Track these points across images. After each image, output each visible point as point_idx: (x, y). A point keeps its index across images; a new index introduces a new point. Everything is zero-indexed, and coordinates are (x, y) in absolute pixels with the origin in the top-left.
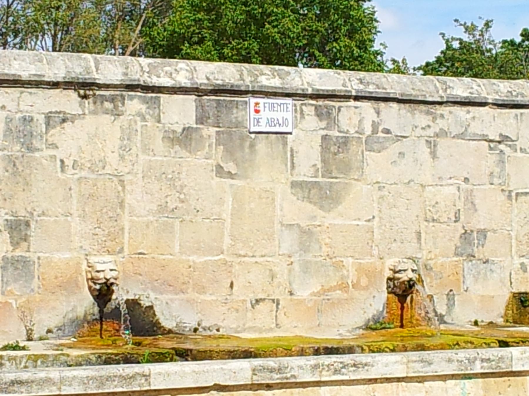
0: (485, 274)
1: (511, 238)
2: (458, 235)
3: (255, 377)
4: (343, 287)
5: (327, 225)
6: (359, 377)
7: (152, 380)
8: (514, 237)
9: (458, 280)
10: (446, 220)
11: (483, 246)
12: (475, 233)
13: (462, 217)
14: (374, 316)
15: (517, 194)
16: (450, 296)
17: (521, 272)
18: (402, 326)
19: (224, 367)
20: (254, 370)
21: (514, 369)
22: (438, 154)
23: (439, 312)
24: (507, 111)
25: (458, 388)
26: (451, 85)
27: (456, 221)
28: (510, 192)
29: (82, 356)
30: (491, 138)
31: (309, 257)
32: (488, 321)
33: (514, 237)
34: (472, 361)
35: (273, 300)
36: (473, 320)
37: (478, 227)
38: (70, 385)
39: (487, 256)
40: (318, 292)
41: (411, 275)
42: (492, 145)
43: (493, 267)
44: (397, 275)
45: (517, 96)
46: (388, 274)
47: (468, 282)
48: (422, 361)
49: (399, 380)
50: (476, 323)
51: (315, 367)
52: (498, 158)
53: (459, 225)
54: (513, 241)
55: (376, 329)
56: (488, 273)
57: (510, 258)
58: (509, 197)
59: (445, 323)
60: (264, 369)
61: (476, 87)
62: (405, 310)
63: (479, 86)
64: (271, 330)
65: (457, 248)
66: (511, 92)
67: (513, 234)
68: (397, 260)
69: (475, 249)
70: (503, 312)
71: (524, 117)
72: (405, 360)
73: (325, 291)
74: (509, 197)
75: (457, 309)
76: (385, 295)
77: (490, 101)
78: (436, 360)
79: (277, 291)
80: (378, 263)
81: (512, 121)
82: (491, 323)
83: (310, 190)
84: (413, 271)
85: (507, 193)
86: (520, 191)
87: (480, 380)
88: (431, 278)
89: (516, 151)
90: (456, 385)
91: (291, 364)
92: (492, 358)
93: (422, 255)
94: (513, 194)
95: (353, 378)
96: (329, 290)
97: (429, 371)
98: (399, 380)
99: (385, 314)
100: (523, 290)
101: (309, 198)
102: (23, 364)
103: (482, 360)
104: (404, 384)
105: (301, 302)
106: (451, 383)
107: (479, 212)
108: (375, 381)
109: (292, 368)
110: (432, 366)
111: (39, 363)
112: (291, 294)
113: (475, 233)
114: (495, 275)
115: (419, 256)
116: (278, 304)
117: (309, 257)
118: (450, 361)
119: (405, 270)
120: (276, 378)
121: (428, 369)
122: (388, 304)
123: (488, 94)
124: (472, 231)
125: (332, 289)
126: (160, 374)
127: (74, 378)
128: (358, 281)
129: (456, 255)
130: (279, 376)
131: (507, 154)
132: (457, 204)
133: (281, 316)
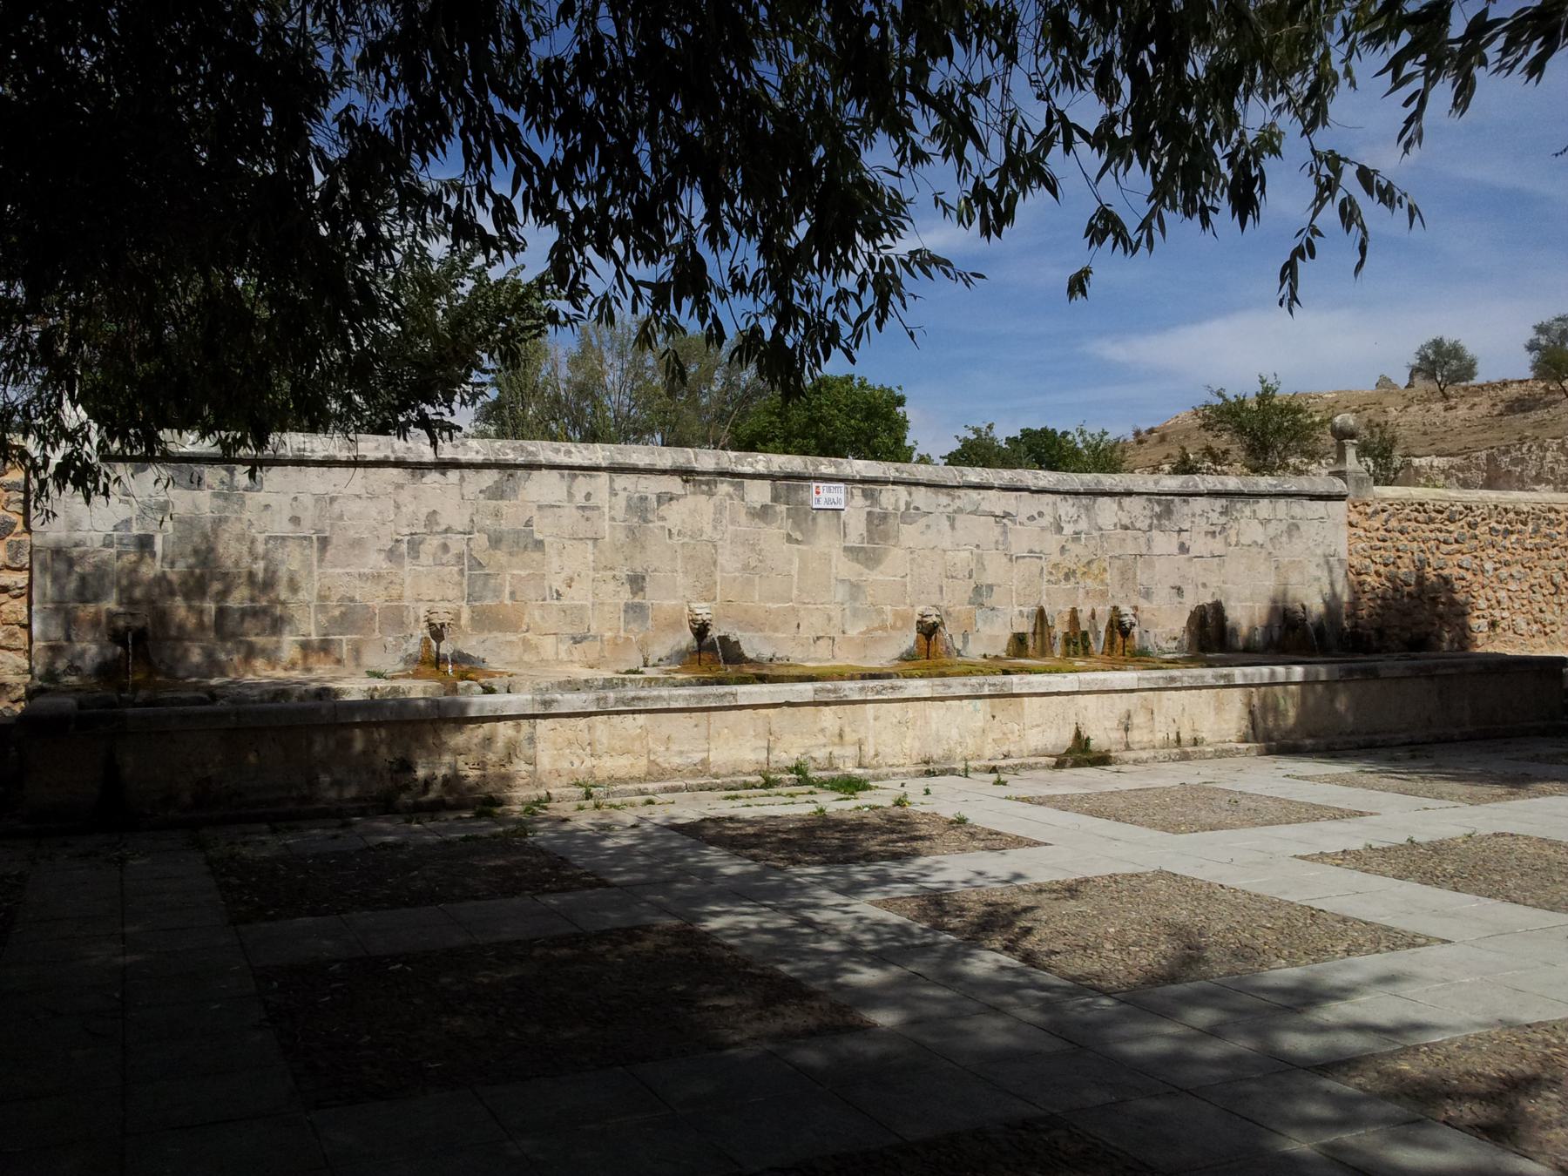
4: (883, 628)
16: (965, 636)
31: (857, 605)
34: (981, 686)
41: (935, 619)
46: (918, 618)
49: (926, 699)
51: (862, 689)
60: (823, 690)
73: (869, 631)
75: (970, 645)
76: (915, 634)
97: (949, 692)
98: (926, 699)
105: (851, 639)
106: (965, 702)
117: (857, 605)
120: (832, 697)
122: (917, 641)
125: (876, 629)
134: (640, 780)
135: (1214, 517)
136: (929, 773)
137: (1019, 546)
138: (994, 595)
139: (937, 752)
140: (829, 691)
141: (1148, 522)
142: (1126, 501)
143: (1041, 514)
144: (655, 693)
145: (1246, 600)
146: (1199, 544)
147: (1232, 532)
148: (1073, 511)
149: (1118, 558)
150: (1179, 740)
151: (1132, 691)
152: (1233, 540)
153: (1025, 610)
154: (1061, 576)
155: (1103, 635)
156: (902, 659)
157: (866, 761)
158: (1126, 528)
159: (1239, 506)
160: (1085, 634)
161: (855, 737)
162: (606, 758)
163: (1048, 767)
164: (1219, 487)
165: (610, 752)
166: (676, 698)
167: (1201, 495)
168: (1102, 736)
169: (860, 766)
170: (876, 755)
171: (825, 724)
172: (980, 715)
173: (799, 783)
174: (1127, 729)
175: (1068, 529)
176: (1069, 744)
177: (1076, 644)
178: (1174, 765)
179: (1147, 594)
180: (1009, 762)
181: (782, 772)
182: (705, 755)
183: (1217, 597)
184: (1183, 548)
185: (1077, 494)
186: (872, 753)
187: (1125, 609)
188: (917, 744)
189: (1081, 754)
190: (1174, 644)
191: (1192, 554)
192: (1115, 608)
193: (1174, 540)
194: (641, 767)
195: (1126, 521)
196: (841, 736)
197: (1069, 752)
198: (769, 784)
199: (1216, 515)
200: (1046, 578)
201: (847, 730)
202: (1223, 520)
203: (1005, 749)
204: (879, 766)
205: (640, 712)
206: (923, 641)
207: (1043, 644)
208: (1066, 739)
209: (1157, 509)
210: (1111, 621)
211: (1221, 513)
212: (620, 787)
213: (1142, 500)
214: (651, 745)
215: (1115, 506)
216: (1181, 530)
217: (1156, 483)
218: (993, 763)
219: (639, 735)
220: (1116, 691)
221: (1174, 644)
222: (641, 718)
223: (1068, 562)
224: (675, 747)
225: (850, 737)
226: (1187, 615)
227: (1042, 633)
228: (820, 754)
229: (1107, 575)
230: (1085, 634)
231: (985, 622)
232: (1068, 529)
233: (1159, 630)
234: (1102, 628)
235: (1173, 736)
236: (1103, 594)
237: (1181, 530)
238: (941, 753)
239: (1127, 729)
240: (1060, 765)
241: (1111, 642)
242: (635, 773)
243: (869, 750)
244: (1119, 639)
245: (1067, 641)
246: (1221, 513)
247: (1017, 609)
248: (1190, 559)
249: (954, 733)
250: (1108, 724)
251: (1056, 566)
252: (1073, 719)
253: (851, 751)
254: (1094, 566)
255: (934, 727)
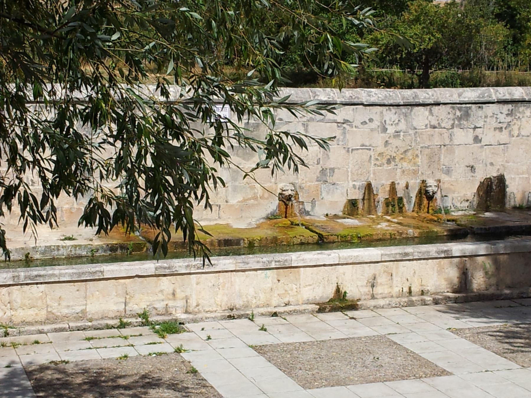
0: (333, 190)
1: (348, 172)
2: (318, 171)
3: (157, 271)
4: (255, 198)
5: (246, 167)
6: (210, 271)
7: (105, 274)
8: (350, 171)
9: (318, 194)
10: (312, 163)
11: (332, 176)
12: (328, 170)
13: (321, 162)
14: (271, 212)
15: (352, 150)
16: (313, 202)
17: (353, 189)
18: (286, 217)
19: (141, 267)
20: (156, 268)
21: (293, 265)
22: (309, 130)
23: (307, 210)
24: (348, 107)
25: (263, 275)
26: (318, 94)
27: (317, 164)
28: (348, 148)
29: (99, 245)
30: (338, 121)
31: (237, 184)
32: (334, 214)
33: (350, 171)
34: (270, 262)
35: (217, 205)
36: (326, 213)
37: (330, 167)
38: (64, 277)
39: (334, 181)
40: (241, 201)
41: (290, 192)
42: (339, 125)
43: (337, 187)
44: (284, 192)
45: (355, 99)
46: (279, 191)
47: (323, 195)
48: (243, 262)
49: (232, 271)
50: (327, 215)
51: (188, 266)
52: (343, 131)
53: (319, 166)
54: (349, 173)
55: (271, 219)
56: (335, 190)
57: (347, 182)
58: (348, 151)
59: (310, 215)
60: (161, 267)
61: (332, 94)
62: (288, 209)
63: (334, 94)
64: (216, 220)
65: (318, 178)
66: (351, 97)
67: (349, 170)
68: (284, 184)
69: (328, 178)
70: (342, 209)
71: (358, 110)
72: (234, 262)
73: (245, 200)
74: (348, 151)
75: (317, 208)
76: (277, 202)
77: (338, 102)
78: (251, 262)
79: (219, 201)
80: (274, 186)
81: (351, 112)
82: (336, 215)
83: (238, 151)
84: (291, 190)
85: (347, 149)
86: (354, 148)
87: (275, 270)
88: (303, 193)
89: (352, 127)
90: (262, 273)
91: (175, 265)
92: (281, 260)
93: (299, 182)
94: (350, 150)
95: (207, 271)
96: (247, 200)
97: (247, 267)
98: (232, 271)
99: (277, 211)
100: (354, 198)
101: (237, 154)
102: (69, 250)
103: (276, 262)
104: (234, 273)
105: (232, 206)
106: (259, 272)
107: (331, 159)
108: (219, 272)
109: (176, 267)
110: (249, 265)
111: (77, 249)
112: (227, 202)
113: (328, 170)
114: (339, 191)
115: (297, 182)
116: (220, 207)
117: (237, 184)
118: (258, 262)
119: (287, 190)
120: (167, 272)
121: (247, 266)
122: (279, 206)
123: (338, 98)
124: (326, 169)
125: (249, 199)
126: (109, 271)
127: (66, 273)
128: (263, 195)
129: (317, 181)
130: (169, 271)
131: (347, 129)
132: (319, 155)
133: (221, 213)
134: (41, 323)
135: (502, 118)
136: (230, 317)
137: (354, 141)
138: (335, 175)
139: (239, 303)
140: (165, 268)
141: (451, 122)
142: (435, 109)
143: (371, 120)
144: (51, 272)
145: (523, 174)
146: (489, 136)
147: (515, 128)
148: (395, 118)
149: (428, 147)
150: (410, 292)
151: (378, 262)
152: (516, 133)
153: (358, 184)
154: (384, 161)
155: (414, 199)
156: (268, 218)
157: (191, 309)
158: (435, 127)
159: (521, 109)
160: (401, 199)
161: (183, 295)
162: (20, 310)
163: (312, 312)
164: (508, 97)
165: (22, 307)
166: (64, 275)
167: (493, 103)
168: (353, 290)
169: (186, 312)
170: (198, 305)
171: (163, 288)
172: (269, 280)
173: (143, 324)
174: (373, 286)
175: (391, 130)
176: (332, 296)
177: (393, 206)
178: (399, 311)
179: (448, 171)
180: (288, 308)
181: (133, 316)
182: (84, 307)
183: (501, 172)
184: (477, 140)
185: (398, 105)
186: (195, 304)
187: (431, 182)
188: (225, 299)
189: (340, 303)
190: (467, 204)
191: (483, 143)
192: (424, 182)
193: (471, 134)
194: (42, 315)
195: (434, 123)
196: (174, 294)
197: (331, 300)
198: (123, 325)
199: (504, 116)
200: (373, 162)
201: (178, 291)
202: (509, 119)
203: (286, 300)
204: (200, 312)
205: (41, 283)
206: (283, 207)
207: (369, 206)
208: (330, 293)
209: (458, 113)
210: (420, 192)
211: (507, 115)
212: (27, 328)
213: (448, 108)
214: (49, 303)
215: (427, 113)
216: (476, 128)
217: (460, 95)
218: (275, 310)
219: (41, 298)
220: (366, 263)
221: (467, 204)
222: (42, 287)
223: (390, 152)
224: (64, 304)
225: (180, 294)
226: (477, 184)
227: (369, 199)
228: (160, 306)
229: (419, 160)
230: (401, 199)
231: (328, 193)
232: (391, 130)
233: (456, 195)
234: (413, 194)
235: (406, 290)
236: (415, 172)
237: (476, 128)
238: (242, 303)
239: (373, 286)
240: (321, 310)
241: (419, 204)
242: (39, 319)
243: (193, 303)
244: (425, 202)
245: (387, 203)
246: (507, 115)
247: (351, 184)
248: (482, 147)
249: (251, 291)
250: (359, 283)
251: (381, 154)
252: (334, 281)
253: (180, 303)
254: (409, 154)
255: (237, 288)
